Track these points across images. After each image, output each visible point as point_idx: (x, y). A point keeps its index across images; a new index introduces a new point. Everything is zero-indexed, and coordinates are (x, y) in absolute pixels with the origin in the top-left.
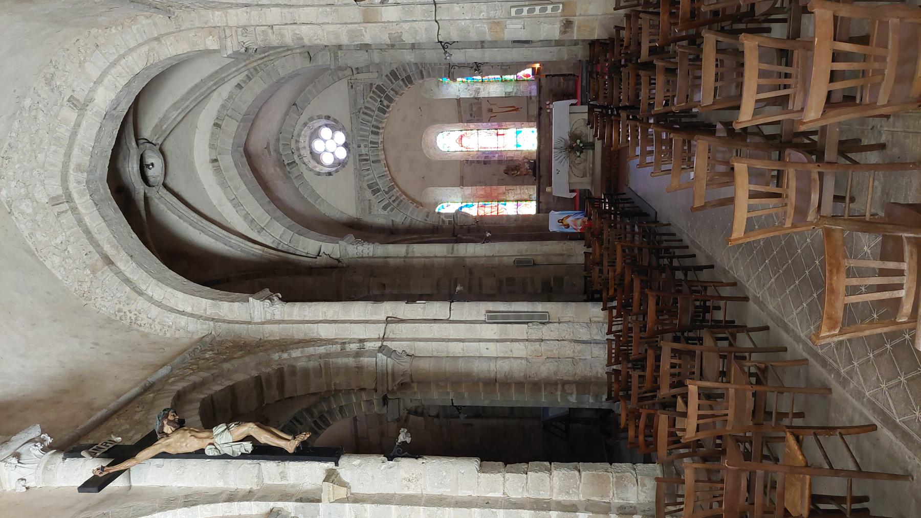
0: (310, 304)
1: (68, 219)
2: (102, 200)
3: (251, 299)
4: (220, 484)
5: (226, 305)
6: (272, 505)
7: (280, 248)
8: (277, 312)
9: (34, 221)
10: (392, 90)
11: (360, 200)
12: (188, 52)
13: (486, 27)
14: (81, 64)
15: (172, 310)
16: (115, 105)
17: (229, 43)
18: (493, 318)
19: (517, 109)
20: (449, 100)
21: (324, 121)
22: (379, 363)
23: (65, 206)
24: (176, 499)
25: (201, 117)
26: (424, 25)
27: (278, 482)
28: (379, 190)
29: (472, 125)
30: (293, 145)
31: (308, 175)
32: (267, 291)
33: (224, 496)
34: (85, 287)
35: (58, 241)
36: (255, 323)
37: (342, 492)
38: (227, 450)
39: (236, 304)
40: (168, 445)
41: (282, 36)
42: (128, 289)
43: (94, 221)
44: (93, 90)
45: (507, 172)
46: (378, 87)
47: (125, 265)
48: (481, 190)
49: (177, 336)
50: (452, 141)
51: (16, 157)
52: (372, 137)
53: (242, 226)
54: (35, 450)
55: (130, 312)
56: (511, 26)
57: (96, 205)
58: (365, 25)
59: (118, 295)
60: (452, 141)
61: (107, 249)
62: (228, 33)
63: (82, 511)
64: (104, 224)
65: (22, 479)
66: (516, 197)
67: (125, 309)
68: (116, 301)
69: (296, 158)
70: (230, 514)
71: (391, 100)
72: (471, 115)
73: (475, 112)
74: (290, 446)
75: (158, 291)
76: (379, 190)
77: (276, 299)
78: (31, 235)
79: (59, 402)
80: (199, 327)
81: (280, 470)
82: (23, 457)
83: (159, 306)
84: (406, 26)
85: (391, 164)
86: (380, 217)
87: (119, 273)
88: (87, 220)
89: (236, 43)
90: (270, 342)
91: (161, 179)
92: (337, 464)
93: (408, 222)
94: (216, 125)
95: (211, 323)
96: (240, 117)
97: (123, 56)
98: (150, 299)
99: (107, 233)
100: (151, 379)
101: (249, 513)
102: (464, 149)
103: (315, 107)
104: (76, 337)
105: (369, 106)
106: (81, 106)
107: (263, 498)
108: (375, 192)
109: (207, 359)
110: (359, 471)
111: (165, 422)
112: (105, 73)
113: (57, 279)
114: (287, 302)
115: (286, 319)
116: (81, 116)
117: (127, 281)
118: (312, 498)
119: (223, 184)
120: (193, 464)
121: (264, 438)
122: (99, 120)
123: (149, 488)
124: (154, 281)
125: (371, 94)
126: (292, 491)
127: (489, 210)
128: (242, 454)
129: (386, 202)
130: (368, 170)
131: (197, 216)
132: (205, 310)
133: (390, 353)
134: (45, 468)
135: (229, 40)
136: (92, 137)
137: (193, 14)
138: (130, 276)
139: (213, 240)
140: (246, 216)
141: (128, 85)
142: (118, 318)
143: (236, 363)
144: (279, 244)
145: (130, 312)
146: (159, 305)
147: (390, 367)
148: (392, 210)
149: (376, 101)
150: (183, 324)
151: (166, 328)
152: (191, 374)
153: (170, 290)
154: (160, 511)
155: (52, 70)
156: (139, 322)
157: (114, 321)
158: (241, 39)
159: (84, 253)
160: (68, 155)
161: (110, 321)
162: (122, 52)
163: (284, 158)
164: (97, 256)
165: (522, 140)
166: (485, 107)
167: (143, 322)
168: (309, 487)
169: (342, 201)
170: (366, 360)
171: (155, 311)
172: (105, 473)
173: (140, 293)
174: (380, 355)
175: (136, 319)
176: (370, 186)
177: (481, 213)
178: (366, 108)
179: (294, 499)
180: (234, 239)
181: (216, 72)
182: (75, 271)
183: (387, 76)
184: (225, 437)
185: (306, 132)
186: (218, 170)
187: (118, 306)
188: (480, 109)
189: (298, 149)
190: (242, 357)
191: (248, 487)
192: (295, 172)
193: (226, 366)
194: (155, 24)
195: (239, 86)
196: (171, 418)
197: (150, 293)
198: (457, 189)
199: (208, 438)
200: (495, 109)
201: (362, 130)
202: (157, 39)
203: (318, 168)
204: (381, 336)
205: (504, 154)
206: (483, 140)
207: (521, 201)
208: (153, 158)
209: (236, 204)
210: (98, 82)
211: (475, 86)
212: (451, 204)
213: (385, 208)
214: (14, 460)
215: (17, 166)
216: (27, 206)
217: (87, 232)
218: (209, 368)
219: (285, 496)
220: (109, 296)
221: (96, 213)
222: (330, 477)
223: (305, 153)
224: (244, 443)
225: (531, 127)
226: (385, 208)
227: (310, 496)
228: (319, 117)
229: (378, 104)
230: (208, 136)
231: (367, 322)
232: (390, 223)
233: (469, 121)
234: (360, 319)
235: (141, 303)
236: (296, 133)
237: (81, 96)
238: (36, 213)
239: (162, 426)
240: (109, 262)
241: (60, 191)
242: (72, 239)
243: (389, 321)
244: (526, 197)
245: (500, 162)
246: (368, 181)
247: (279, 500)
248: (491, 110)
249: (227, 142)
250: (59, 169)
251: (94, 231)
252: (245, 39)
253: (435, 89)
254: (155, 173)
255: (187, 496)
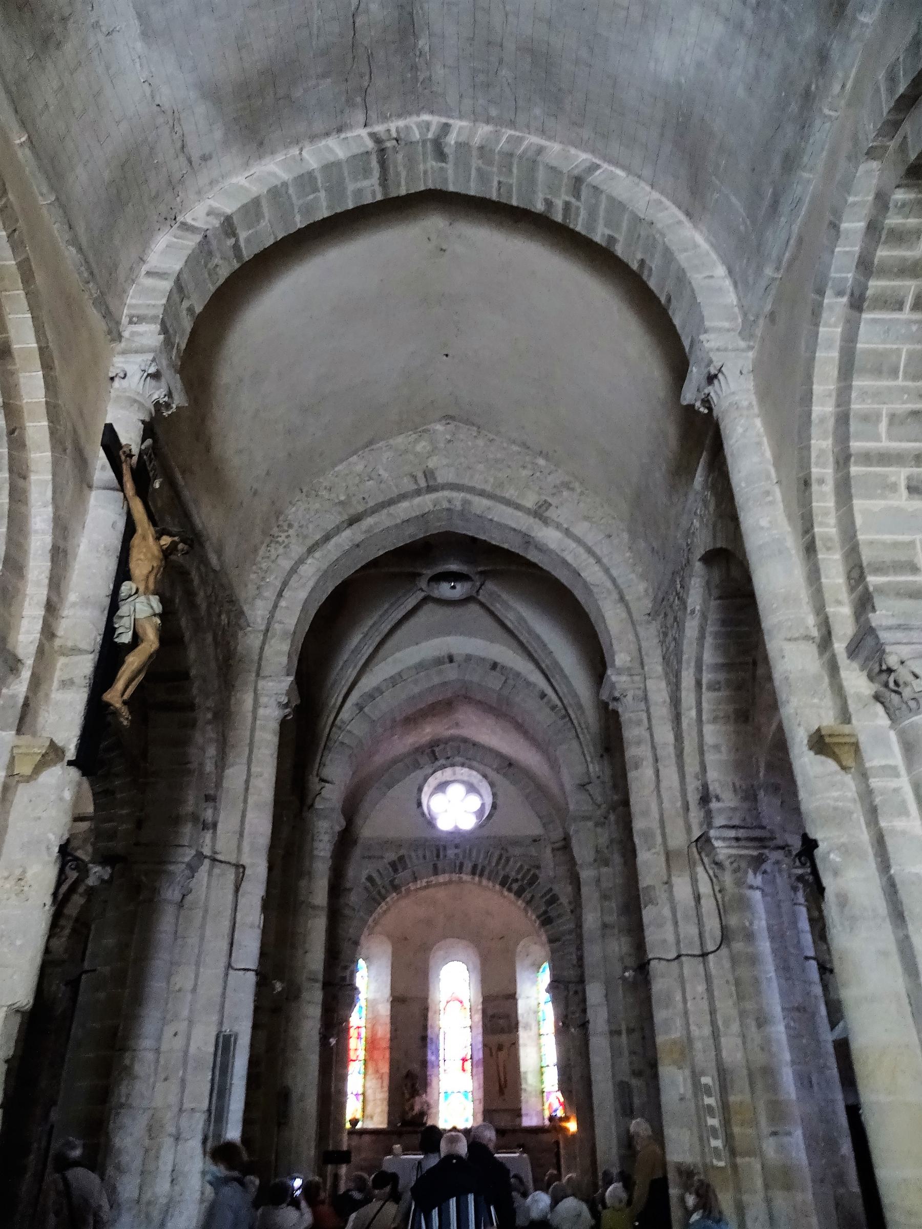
0: (275, 755)
1: (408, 485)
2: (427, 522)
3: (291, 678)
4: (72, 597)
5: (285, 647)
6: (29, 662)
7: (334, 729)
8: (268, 711)
9: (406, 451)
10: (533, 897)
11: (387, 844)
12: (608, 632)
13: (676, 1034)
14: (586, 518)
15: (285, 584)
16: (541, 548)
17: (624, 678)
18: (224, 1044)
19: (501, 1091)
20: (513, 981)
21: (489, 800)
22: (180, 850)
23: (423, 484)
24: (65, 538)
25: (503, 648)
26: (670, 938)
27: (58, 675)
28: (396, 870)
29: (478, 1017)
30: (458, 759)
31: (419, 774)
32: (296, 701)
33: (55, 599)
34: (324, 493)
35: (381, 472)
36: (256, 682)
37: (24, 768)
38: (124, 609)
39: (285, 660)
40: (144, 538)
41: (639, 743)
42: (318, 537)
43: (404, 510)
44: (558, 526)
45: (410, 1076)
46: (535, 878)
47: (346, 538)
48: (384, 1031)
49: (250, 586)
50: (455, 987)
51: (480, 442)
52: (468, 866)
53: (368, 683)
54: (159, 394)
55: (288, 537)
56: (681, 1079)
57: (423, 516)
58: (662, 852)
59: (311, 526)
60: (455, 987)
61: (369, 521)
62: (637, 678)
63: (75, 431)
64: (399, 521)
65: (125, 375)
66: (369, 1093)
67: (291, 532)
68: (303, 522)
69: (442, 761)
70: (26, 604)
71: (519, 894)
72: (493, 1016)
73: (499, 1023)
74: (115, 696)
75: (311, 570)
76: (396, 870)
77: (288, 710)
78: (390, 447)
79: (197, 440)
80: (259, 612)
81: (76, 680)
82: (154, 383)
83: (292, 569)
84: (667, 912)
85: (431, 891)
86: (359, 871)
87: (338, 530)
88: (405, 504)
89: (625, 686)
90: (229, 698)
91: (436, 594)
92: (70, 763)
93: (347, 912)
94: (494, 666)
95: (263, 627)
96: (505, 692)
97: (599, 561)
98: (301, 561)
99: (388, 523)
100: (207, 545)
101: (23, 630)
102: (442, 1006)
103: (508, 788)
104: (268, 473)
105: (511, 863)
106: (540, 513)
107: (41, 652)
108: (394, 865)
109: (219, 616)
110: (53, 797)
111: (176, 539)
112: (578, 541)
113: (334, 465)
114: (280, 725)
115: (258, 722)
116: (528, 511)
117: (327, 538)
118: (25, 719)
119: (421, 666)
120: (110, 565)
121: (133, 662)
122: (524, 529)
123: (85, 512)
124: (325, 567)
125: (526, 868)
126: (41, 694)
127: (357, 1046)
128: (115, 629)
129: (378, 881)
130: (424, 857)
131: (386, 630)
132: (280, 622)
133: (193, 868)
134: (135, 401)
135: (629, 678)
136: (502, 521)
137: (656, 641)
138: (333, 541)
139: (353, 647)
140: (378, 690)
141: (565, 563)
142: (281, 523)
143: (211, 650)
144: (340, 728)
145: (288, 537)
146: (293, 570)
147: (172, 868)
148: (366, 888)
149: (518, 872)
150: (266, 594)
151: (261, 574)
152: (205, 593)
153: (311, 584)
154: (55, 514)
155: (579, 490)
156: (273, 545)
157: (278, 518)
158: (630, 694)
159: (366, 496)
160: (482, 493)
161: (278, 514)
162: (605, 560)
163: (442, 746)
164: (361, 509)
165: (455, 1104)
166: (503, 1038)
167: (273, 550)
168: (41, 720)
169: (379, 822)
170: (187, 829)
171: (287, 564)
172: (123, 458)
173: (311, 550)
174: (193, 852)
175: (277, 542)
176: (401, 858)
177: (353, 1032)
178: (508, 860)
179: (30, 695)
180: (352, 673)
181: (562, 670)
182: (344, 484)
183: (551, 890)
184: (142, 609)
185: (475, 777)
186: (438, 661)
187: (296, 525)
188: (502, 1031)
189: (453, 765)
190: (217, 660)
191: (60, 632)
192: (423, 759)
193: (209, 638)
194: (639, 599)
195: (543, 695)
196: (181, 546)
197: (309, 561)
198: (386, 992)
199: (147, 588)
200: (502, 1055)
201: (479, 852)
202: (622, 599)
203: (427, 790)
204: (219, 857)
205: (435, 1070)
206: (456, 1030)
207: (364, 1101)
208: (459, 590)
209: (394, 681)
210: (567, 532)
211: (534, 1024)
212: (371, 983)
213: (370, 879)
214: (152, 370)
215: (470, 443)
216: (424, 447)
217: (391, 502)
218: (209, 614)
219: (36, 682)
220: (309, 515)
221: (414, 514)
222: (54, 752)
223: (447, 774)
224: (131, 633)
225: (474, 1116)
226: (370, 879)
227: (28, 719)
228: (494, 795)
229: (513, 874)
230: (482, 654)
231: (241, 835)
232: (348, 885)
233: (484, 1012)
234: (247, 826)
235: (297, 550)
236: (475, 764)
237: (551, 513)
238: (416, 455)
239: (171, 535)
240: (353, 521)
241: (440, 480)
242: (383, 486)
243: (240, 869)
244: (369, 1109)
245: (424, 1064)
246: (410, 857)
247: (33, 674)
248: (500, 1048)
249: (474, 676)
250: (466, 481)
251: (392, 509)
252: (629, 698)
253: (528, 961)
254: (445, 590)
255: (65, 552)
